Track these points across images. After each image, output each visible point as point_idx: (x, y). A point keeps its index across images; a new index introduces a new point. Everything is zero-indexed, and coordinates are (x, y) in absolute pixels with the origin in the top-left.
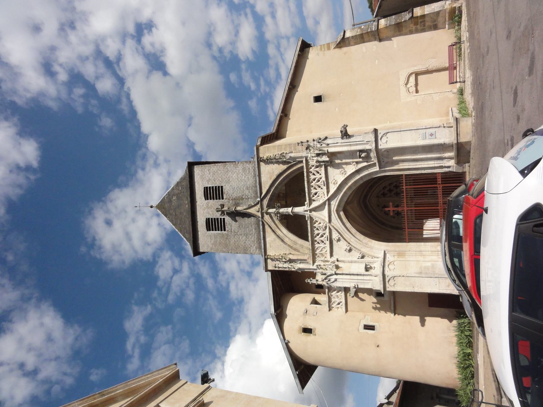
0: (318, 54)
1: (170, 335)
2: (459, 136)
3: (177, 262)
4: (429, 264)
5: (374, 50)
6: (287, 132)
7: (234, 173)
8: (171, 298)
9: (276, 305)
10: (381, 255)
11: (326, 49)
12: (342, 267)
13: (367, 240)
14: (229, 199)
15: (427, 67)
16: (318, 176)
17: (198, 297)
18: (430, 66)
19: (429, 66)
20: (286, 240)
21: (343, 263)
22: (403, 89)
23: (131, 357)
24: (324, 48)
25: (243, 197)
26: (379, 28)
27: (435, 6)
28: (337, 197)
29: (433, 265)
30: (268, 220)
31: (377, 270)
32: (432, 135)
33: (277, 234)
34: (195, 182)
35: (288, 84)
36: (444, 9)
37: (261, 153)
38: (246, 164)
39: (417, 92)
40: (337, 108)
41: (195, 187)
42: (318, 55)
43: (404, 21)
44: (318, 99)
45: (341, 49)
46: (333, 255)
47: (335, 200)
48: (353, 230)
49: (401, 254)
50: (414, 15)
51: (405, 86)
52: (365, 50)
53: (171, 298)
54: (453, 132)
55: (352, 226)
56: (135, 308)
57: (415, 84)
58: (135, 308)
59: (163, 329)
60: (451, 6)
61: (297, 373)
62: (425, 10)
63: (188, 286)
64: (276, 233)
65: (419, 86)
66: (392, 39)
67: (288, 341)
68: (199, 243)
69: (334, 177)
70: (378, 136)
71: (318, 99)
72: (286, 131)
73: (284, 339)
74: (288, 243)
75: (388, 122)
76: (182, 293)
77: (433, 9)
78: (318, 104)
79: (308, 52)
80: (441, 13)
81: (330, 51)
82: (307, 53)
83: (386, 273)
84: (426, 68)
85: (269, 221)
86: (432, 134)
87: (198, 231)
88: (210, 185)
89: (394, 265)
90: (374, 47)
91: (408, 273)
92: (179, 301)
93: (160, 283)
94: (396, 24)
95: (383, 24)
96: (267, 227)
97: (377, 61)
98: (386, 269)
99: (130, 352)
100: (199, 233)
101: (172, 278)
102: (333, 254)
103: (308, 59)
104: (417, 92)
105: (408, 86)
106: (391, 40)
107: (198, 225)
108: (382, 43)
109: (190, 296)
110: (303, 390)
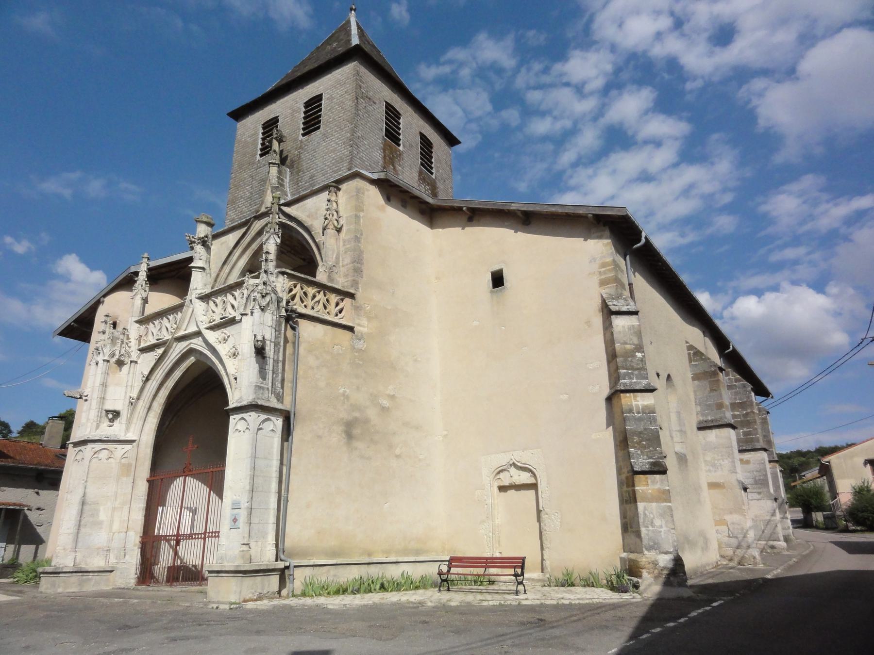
0: (593, 260)
1: (479, 113)
2: (216, 575)
3: (598, 83)
4: (103, 516)
5: (591, 387)
6: (440, 230)
7: (336, 143)
8: (534, 96)
9: (163, 270)
10: (130, 437)
11: (603, 277)
12: (120, 371)
13: (157, 410)
14: (301, 147)
15: (545, 510)
16: (332, 308)
17: (545, 138)
18: (546, 516)
19: (547, 514)
20: (227, 269)
21: (127, 373)
22: (503, 460)
23: (438, 64)
24: (605, 273)
25: (300, 174)
26: (621, 394)
27: (661, 527)
28: (206, 347)
29: (101, 523)
30: (255, 229)
31: (106, 430)
32: (235, 520)
33: (235, 251)
34: (331, 73)
35: (523, 207)
36: (644, 549)
37: (348, 185)
38: (348, 161)
39: (502, 489)
40: (478, 322)
41: (323, 77)
42: (591, 262)
43: (629, 452)
44: (498, 280)
45: (599, 311)
46: (143, 353)
47: (203, 343)
48: (170, 384)
49: (127, 469)
50: (638, 478)
51: (511, 462)
52: (590, 367)
53: (534, 96)
54: (232, 564)
55: (176, 380)
56: (509, 41)
57: (517, 484)
58: (509, 41)
59: (485, 96)
60: (647, 566)
61: (72, 324)
62: (652, 502)
63: (555, 118)
64: (236, 249)
65: (516, 492)
66: (611, 428)
67: (103, 302)
68: (248, 117)
69: (233, 335)
70: (246, 412)
71: (498, 280)
72: (443, 228)
73: (105, 296)
74: (222, 273)
75: (445, 433)
76: (543, 114)
77: (652, 523)
78: (488, 281)
79: (600, 237)
80: (638, 540)
81: (597, 285)
82: (599, 234)
83: (90, 446)
84: (543, 508)
85: (252, 232)
86: (234, 519)
87: (263, 109)
88: (324, 106)
89: (107, 457)
90: (598, 387)
91: (241, 480)
92: (530, 112)
93: (558, 67)
94: (626, 431)
95: (634, 403)
96: (243, 230)
97: (565, 397)
98: (98, 446)
99: (442, 60)
100: (261, 112)
101: (567, 84)
102: (144, 354)
103: (585, 240)
104: (502, 489)
105: (513, 470)
106: (608, 426)
107: (271, 104)
108: (603, 404)
109: (541, 127)
110: (58, 335)
